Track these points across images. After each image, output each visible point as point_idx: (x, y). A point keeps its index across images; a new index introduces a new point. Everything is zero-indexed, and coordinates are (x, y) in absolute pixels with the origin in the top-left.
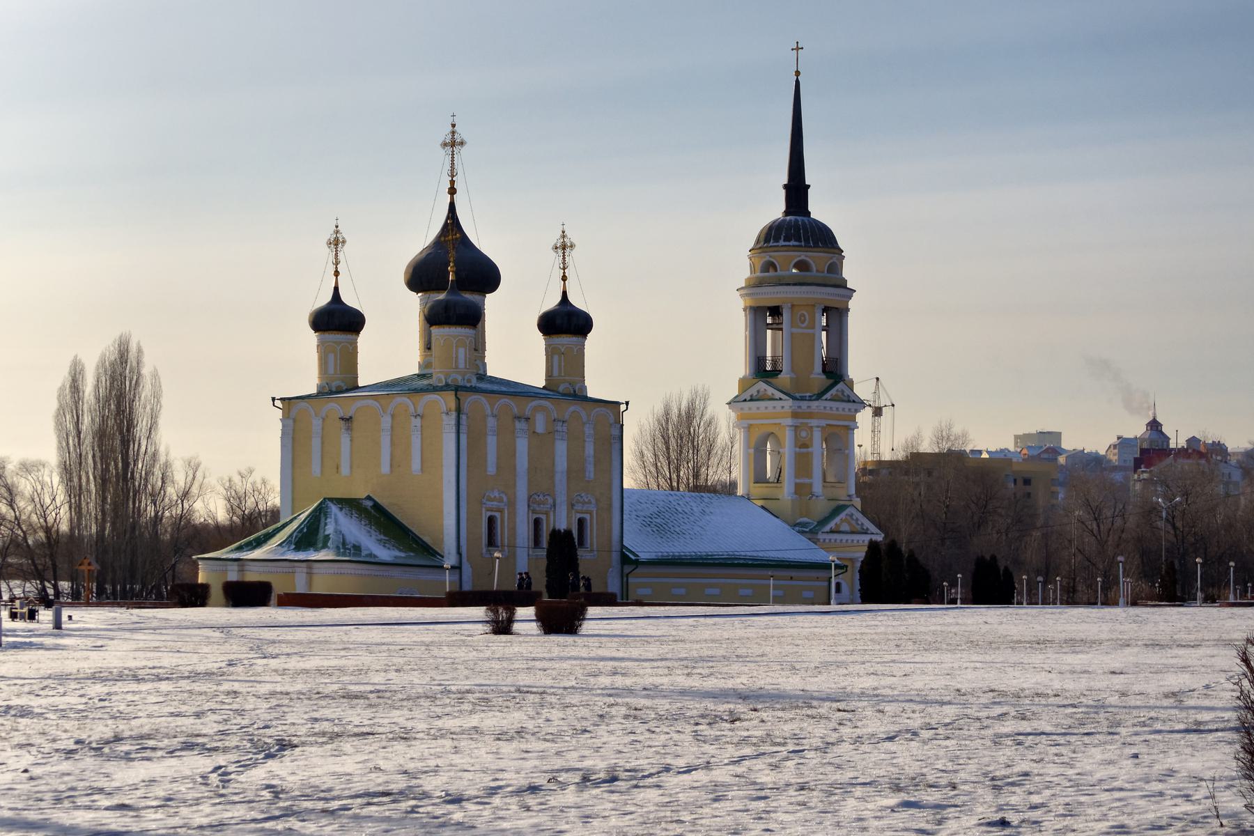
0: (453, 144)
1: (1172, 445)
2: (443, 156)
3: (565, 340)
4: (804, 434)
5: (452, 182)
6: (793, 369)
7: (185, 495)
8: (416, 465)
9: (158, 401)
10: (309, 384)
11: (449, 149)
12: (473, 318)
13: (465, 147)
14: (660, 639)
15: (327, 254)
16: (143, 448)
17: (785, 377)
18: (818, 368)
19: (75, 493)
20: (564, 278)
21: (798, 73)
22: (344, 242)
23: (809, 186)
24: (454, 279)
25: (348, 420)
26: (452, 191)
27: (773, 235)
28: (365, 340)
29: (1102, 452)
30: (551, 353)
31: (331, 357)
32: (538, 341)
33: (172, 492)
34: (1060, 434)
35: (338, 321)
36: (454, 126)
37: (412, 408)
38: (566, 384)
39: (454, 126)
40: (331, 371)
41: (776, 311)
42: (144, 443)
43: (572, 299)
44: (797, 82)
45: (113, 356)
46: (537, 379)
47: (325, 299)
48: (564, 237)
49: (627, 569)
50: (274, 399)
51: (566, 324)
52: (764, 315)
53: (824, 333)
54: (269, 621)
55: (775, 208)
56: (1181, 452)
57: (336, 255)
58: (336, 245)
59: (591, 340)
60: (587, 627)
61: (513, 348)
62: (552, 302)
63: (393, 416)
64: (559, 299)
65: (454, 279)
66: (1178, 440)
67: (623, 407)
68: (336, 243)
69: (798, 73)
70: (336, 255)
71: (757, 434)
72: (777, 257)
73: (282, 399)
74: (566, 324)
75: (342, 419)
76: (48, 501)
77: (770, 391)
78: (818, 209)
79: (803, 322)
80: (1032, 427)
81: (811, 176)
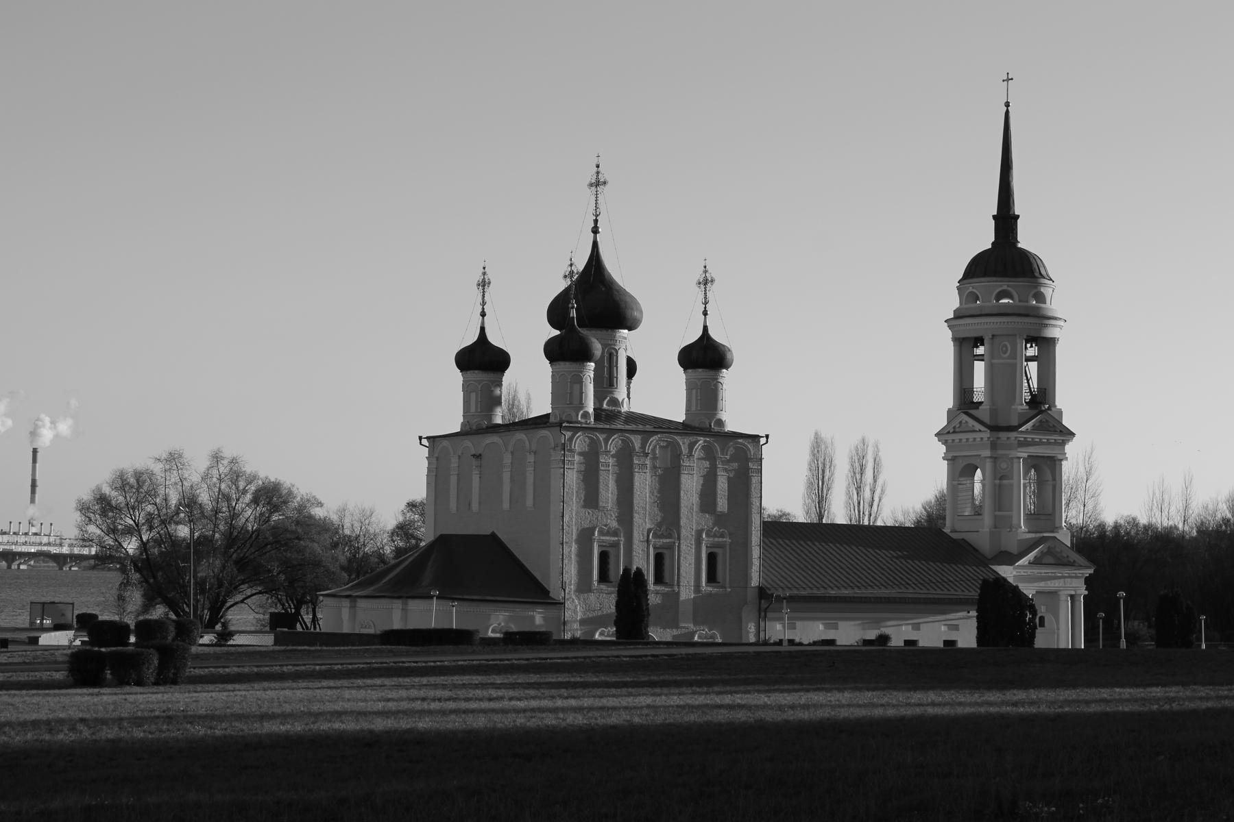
2: (589, 194)
3: (701, 373)
5: (596, 221)
8: (529, 502)
10: (452, 422)
20: (705, 313)
21: (1007, 105)
24: (591, 310)
25: (478, 457)
26: (595, 231)
27: (979, 267)
31: (473, 396)
32: (678, 378)
35: (483, 360)
36: (598, 166)
38: (703, 420)
39: (598, 166)
40: (473, 409)
43: (712, 333)
44: (1007, 113)
47: (471, 338)
48: (706, 272)
50: (420, 438)
51: (704, 358)
52: (965, 345)
55: (985, 238)
58: (705, 284)
59: (726, 376)
62: (694, 335)
63: (512, 453)
64: (700, 333)
65: (591, 310)
67: (763, 441)
68: (484, 284)
69: (1007, 105)
71: (961, 464)
73: (428, 438)
74: (704, 358)
75: (474, 456)
77: (971, 422)
78: (1026, 239)
81: (1020, 206)
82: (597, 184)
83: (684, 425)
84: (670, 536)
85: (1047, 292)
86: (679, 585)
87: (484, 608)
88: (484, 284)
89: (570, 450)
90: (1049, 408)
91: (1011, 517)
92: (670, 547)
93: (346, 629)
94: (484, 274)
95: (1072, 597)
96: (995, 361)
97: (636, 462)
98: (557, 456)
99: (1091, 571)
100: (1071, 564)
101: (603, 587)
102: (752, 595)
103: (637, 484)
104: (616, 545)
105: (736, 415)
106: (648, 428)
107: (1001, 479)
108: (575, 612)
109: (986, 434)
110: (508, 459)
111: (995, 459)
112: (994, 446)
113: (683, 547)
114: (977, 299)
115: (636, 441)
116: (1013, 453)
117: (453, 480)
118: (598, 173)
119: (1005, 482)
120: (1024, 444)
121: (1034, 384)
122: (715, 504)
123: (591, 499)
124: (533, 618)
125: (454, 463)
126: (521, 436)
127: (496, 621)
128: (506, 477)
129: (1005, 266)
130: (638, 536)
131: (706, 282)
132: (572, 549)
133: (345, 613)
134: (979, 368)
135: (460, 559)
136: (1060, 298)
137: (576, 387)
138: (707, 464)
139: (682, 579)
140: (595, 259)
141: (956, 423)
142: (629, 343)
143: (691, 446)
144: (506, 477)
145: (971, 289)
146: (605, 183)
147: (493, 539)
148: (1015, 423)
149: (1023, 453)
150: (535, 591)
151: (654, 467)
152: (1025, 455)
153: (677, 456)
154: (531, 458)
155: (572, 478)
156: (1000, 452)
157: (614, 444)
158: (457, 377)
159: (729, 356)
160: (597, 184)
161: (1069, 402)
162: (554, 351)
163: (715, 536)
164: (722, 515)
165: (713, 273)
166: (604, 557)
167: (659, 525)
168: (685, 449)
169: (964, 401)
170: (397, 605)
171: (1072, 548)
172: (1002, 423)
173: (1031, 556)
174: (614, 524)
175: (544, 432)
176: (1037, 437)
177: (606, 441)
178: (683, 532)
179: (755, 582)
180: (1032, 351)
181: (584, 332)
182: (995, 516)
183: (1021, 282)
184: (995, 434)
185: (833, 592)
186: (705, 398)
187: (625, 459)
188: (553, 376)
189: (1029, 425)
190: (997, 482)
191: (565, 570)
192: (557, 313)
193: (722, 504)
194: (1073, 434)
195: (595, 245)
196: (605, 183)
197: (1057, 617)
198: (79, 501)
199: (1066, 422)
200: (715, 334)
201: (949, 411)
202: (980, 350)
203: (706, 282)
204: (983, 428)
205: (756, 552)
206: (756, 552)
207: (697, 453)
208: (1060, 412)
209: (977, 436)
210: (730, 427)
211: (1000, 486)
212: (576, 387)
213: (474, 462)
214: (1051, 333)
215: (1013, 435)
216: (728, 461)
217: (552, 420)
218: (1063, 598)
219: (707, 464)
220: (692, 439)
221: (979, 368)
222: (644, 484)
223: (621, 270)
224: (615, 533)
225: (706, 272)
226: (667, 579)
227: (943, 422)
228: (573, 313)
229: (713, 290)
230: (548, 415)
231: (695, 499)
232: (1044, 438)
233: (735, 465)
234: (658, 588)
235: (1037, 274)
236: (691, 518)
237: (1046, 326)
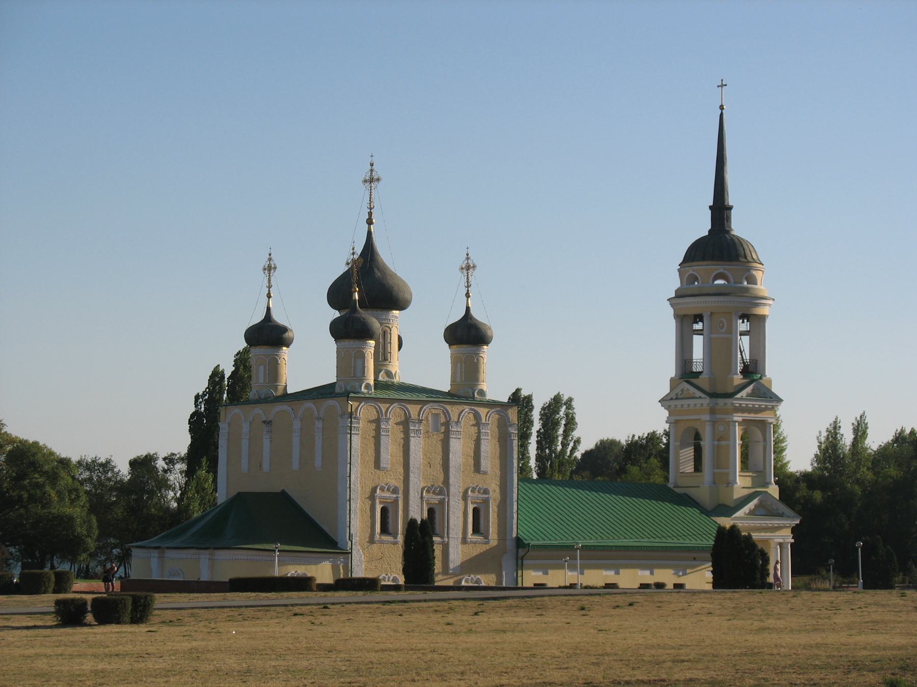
0: (371, 180)
2: (363, 190)
3: (465, 349)
4: (721, 428)
5: (370, 214)
8: (318, 462)
11: (367, 184)
13: (381, 182)
15: (263, 278)
17: (702, 381)
21: (722, 108)
22: (275, 268)
23: (730, 208)
24: (365, 296)
25: (268, 423)
26: (370, 222)
27: (698, 253)
30: (455, 361)
31: (459, 365)
32: (445, 352)
36: (372, 165)
39: (372, 165)
43: (474, 313)
44: (721, 115)
47: (259, 317)
48: (468, 259)
49: (521, 552)
51: (467, 335)
52: (686, 322)
54: (459, 597)
55: (702, 227)
57: (269, 280)
58: (270, 270)
59: (487, 353)
60: (156, 616)
61: (417, 354)
62: (457, 315)
65: (365, 296)
68: (269, 269)
69: (722, 108)
70: (269, 280)
72: (690, 271)
74: (467, 335)
75: (264, 422)
77: (692, 390)
78: (739, 227)
79: (722, 327)
81: (732, 199)
82: (371, 180)
83: (449, 394)
85: (758, 275)
86: (448, 537)
88: (269, 269)
89: (355, 418)
90: (761, 378)
91: (728, 474)
93: (155, 576)
94: (270, 259)
96: (713, 336)
97: (412, 428)
99: (798, 522)
100: (781, 515)
101: (385, 538)
102: (510, 545)
107: (718, 440)
109: (706, 401)
110: (297, 425)
111: (714, 423)
112: (713, 411)
113: (452, 503)
114: (696, 279)
117: (245, 444)
118: (372, 170)
119: (723, 443)
120: (741, 410)
121: (747, 356)
125: (246, 427)
126: (309, 404)
128: (296, 441)
129: (719, 252)
131: (468, 268)
133: (154, 562)
134: (698, 343)
137: (359, 362)
139: (451, 531)
140: (369, 247)
141: (678, 390)
142: (399, 322)
144: (296, 441)
145: (691, 272)
146: (378, 180)
147: (283, 497)
149: (738, 417)
154: (319, 424)
156: (718, 416)
159: (489, 333)
160: (371, 180)
161: (775, 373)
162: (339, 331)
165: (474, 259)
166: (384, 511)
168: (454, 418)
169: (686, 372)
170: (204, 557)
172: (720, 390)
175: (331, 402)
180: (743, 326)
181: (363, 314)
182: (714, 474)
184: (714, 400)
186: (467, 373)
188: (338, 352)
189: (744, 393)
190: (716, 443)
192: (338, 294)
194: (781, 400)
195: (369, 233)
196: (378, 180)
198: (654, 432)
199: (775, 389)
200: (477, 314)
201: (672, 380)
202: (698, 326)
203: (468, 268)
204: (703, 395)
208: (770, 381)
212: (359, 362)
215: (728, 401)
217: (337, 390)
218: (773, 545)
220: (460, 408)
221: (698, 343)
223: (394, 259)
225: (468, 259)
227: (665, 390)
229: (275, 275)
230: (332, 385)
235: (749, 258)
237: (758, 305)
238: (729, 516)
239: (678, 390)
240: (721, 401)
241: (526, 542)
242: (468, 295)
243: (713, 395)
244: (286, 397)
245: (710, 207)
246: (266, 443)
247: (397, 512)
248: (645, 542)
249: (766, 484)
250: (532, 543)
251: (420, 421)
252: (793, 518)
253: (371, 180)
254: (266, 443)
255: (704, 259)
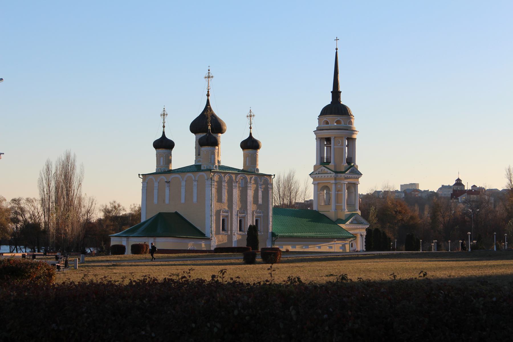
1: (466, 189)
2: (205, 81)
3: (250, 151)
4: (339, 186)
5: (208, 92)
6: (334, 162)
7: (88, 212)
8: (195, 200)
9: (83, 176)
11: (207, 79)
12: (215, 143)
14: (107, 261)
16: (75, 194)
17: (331, 165)
18: (345, 161)
19: (47, 211)
21: (337, 49)
23: (340, 92)
24: (207, 128)
25: (168, 182)
26: (208, 95)
27: (326, 111)
28: (174, 152)
29: (436, 191)
31: (248, 158)
33: (84, 210)
34: (418, 184)
35: (164, 145)
36: (209, 70)
37: (193, 178)
38: (250, 168)
39: (209, 70)
41: (328, 140)
42: (76, 191)
44: (336, 52)
45: (63, 158)
46: (239, 165)
50: (139, 175)
51: (250, 145)
53: (347, 148)
55: (328, 100)
56: (469, 192)
57: (164, 119)
59: (260, 152)
61: (229, 154)
64: (248, 136)
65: (207, 128)
66: (468, 187)
67: (273, 177)
69: (337, 49)
70: (164, 119)
72: (328, 118)
74: (250, 145)
75: (166, 182)
76: (36, 214)
77: (326, 170)
78: (344, 100)
79: (339, 143)
80: (407, 181)
83: (243, 171)
84: (244, 213)
87: (187, 240)
91: (342, 206)
92: (244, 217)
95: (361, 235)
98: (208, 182)
99: (368, 226)
100: (361, 223)
102: (269, 235)
103: (234, 193)
104: (227, 216)
105: (263, 168)
106: (236, 172)
108: (215, 242)
109: (333, 174)
111: (336, 184)
112: (335, 179)
113: (248, 217)
115: (234, 176)
116: (342, 182)
117: (156, 191)
119: (339, 193)
122: (258, 201)
123: (220, 200)
124: (201, 244)
125: (156, 184)
127: (190, 245)
128: (183, 191)
129: (336, 110)
130: (234, 213)
132: (214, 218)
135: (162, 223)
136: (358, 123)
138: (255, 186)
143: (251, 178)
144: (183, 191)
148: (343, 170)
150: (200, 235)
151: (239, 187)
152: (347, 182)
153: (246, 183)
154: (195, 183)
155: (214, 190)
156: (338, 181)
157: (227, 178)
158: (154, 151)
161: (360, 162)
163: (258, 213)
164: (260, 205)
166: (223, 220)
167: (240, 209)
171: (362, 215)
172: (338, 170)
173: (350, 220)
174: (227, 209)
176: (351, 176)
177: (224, 176)
178: (248, 212)
179: (270, 231)
181: (214, 135)
183: (344, 117)
185: (295, 234)
187: (230, 183)
191: (211, 226)
193: (260, 201)
195: (208, 101)
196: (206, 77)
197: (356, 243)
199: (359, 169)
200: (254, 136)
201: (315, 166)
205: (271, 219)
206: (271, 219)
207: (253, 182)
208: (357, 166)
209: (329, 175)
210: (261, 172)
211: (338, 194)
213: (166, 184)
214: (355, 136)
215: (343, 175)
216: (262, 185)
219: (255, 186)
220: (251, 176)
222: (236, 193)
224: (227, 212)
226: (226, 229)
228: (209, 128)
229: (253, 120)
231: (252, 199)
232: (353, 176)
233: (264, 186)
234: (241, 233)
236: (251, 207)
237: (353, 134)
238: (344, 224)
239: (320, 170)
240: (339, 175)
241: (277, 234)
242: (251, 128)
243: (336, 172)
244: (171, 172)
245: (332, 92)
246: (167, 191)
247: (228, 221)
248: (319, 235)
249: (356, 210)
250: (279, 235)
251: (237, 182)
252: (367, 225)
253: (209, 77)
254: (167, 191)
255: (331, 114)
